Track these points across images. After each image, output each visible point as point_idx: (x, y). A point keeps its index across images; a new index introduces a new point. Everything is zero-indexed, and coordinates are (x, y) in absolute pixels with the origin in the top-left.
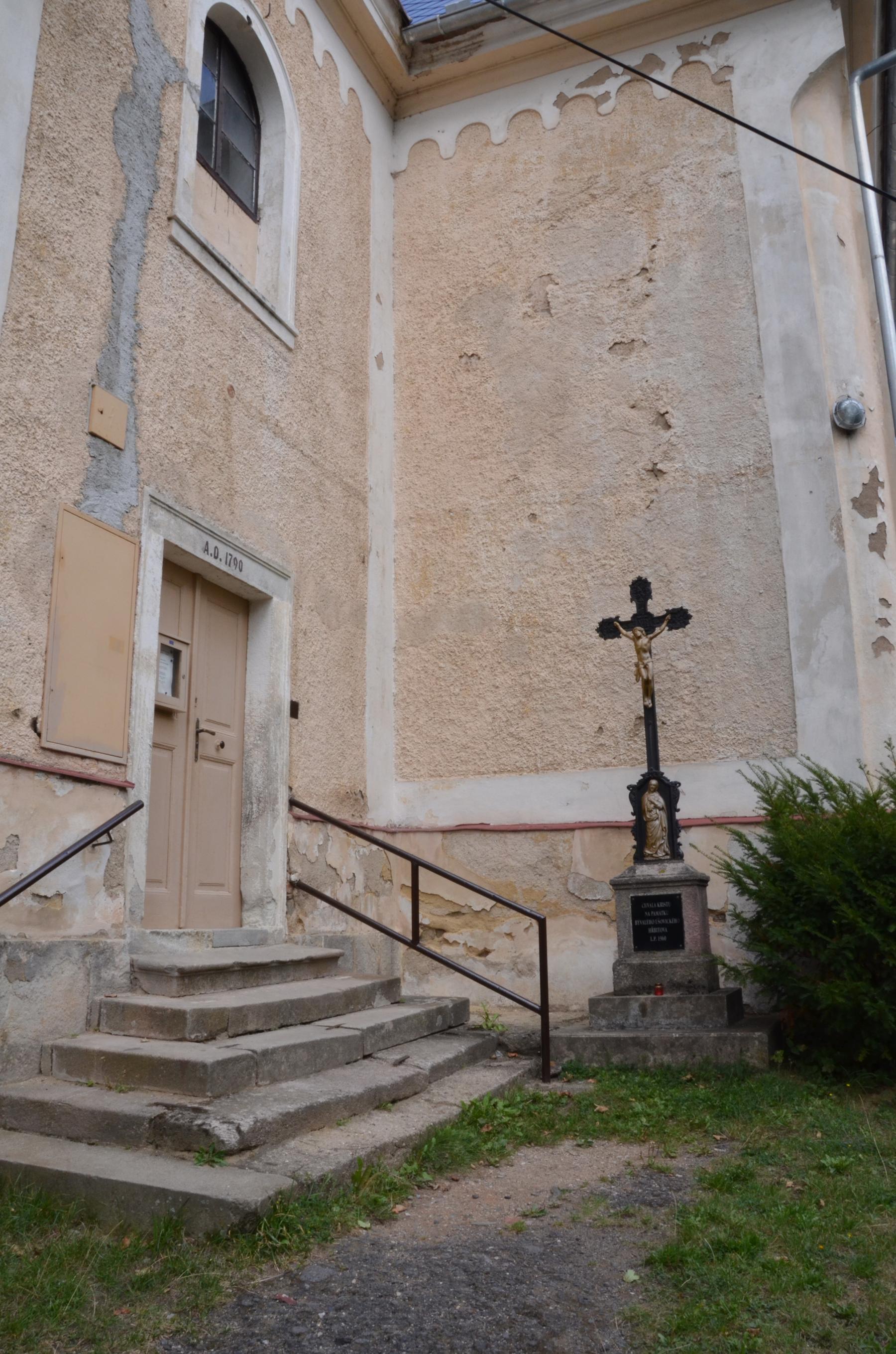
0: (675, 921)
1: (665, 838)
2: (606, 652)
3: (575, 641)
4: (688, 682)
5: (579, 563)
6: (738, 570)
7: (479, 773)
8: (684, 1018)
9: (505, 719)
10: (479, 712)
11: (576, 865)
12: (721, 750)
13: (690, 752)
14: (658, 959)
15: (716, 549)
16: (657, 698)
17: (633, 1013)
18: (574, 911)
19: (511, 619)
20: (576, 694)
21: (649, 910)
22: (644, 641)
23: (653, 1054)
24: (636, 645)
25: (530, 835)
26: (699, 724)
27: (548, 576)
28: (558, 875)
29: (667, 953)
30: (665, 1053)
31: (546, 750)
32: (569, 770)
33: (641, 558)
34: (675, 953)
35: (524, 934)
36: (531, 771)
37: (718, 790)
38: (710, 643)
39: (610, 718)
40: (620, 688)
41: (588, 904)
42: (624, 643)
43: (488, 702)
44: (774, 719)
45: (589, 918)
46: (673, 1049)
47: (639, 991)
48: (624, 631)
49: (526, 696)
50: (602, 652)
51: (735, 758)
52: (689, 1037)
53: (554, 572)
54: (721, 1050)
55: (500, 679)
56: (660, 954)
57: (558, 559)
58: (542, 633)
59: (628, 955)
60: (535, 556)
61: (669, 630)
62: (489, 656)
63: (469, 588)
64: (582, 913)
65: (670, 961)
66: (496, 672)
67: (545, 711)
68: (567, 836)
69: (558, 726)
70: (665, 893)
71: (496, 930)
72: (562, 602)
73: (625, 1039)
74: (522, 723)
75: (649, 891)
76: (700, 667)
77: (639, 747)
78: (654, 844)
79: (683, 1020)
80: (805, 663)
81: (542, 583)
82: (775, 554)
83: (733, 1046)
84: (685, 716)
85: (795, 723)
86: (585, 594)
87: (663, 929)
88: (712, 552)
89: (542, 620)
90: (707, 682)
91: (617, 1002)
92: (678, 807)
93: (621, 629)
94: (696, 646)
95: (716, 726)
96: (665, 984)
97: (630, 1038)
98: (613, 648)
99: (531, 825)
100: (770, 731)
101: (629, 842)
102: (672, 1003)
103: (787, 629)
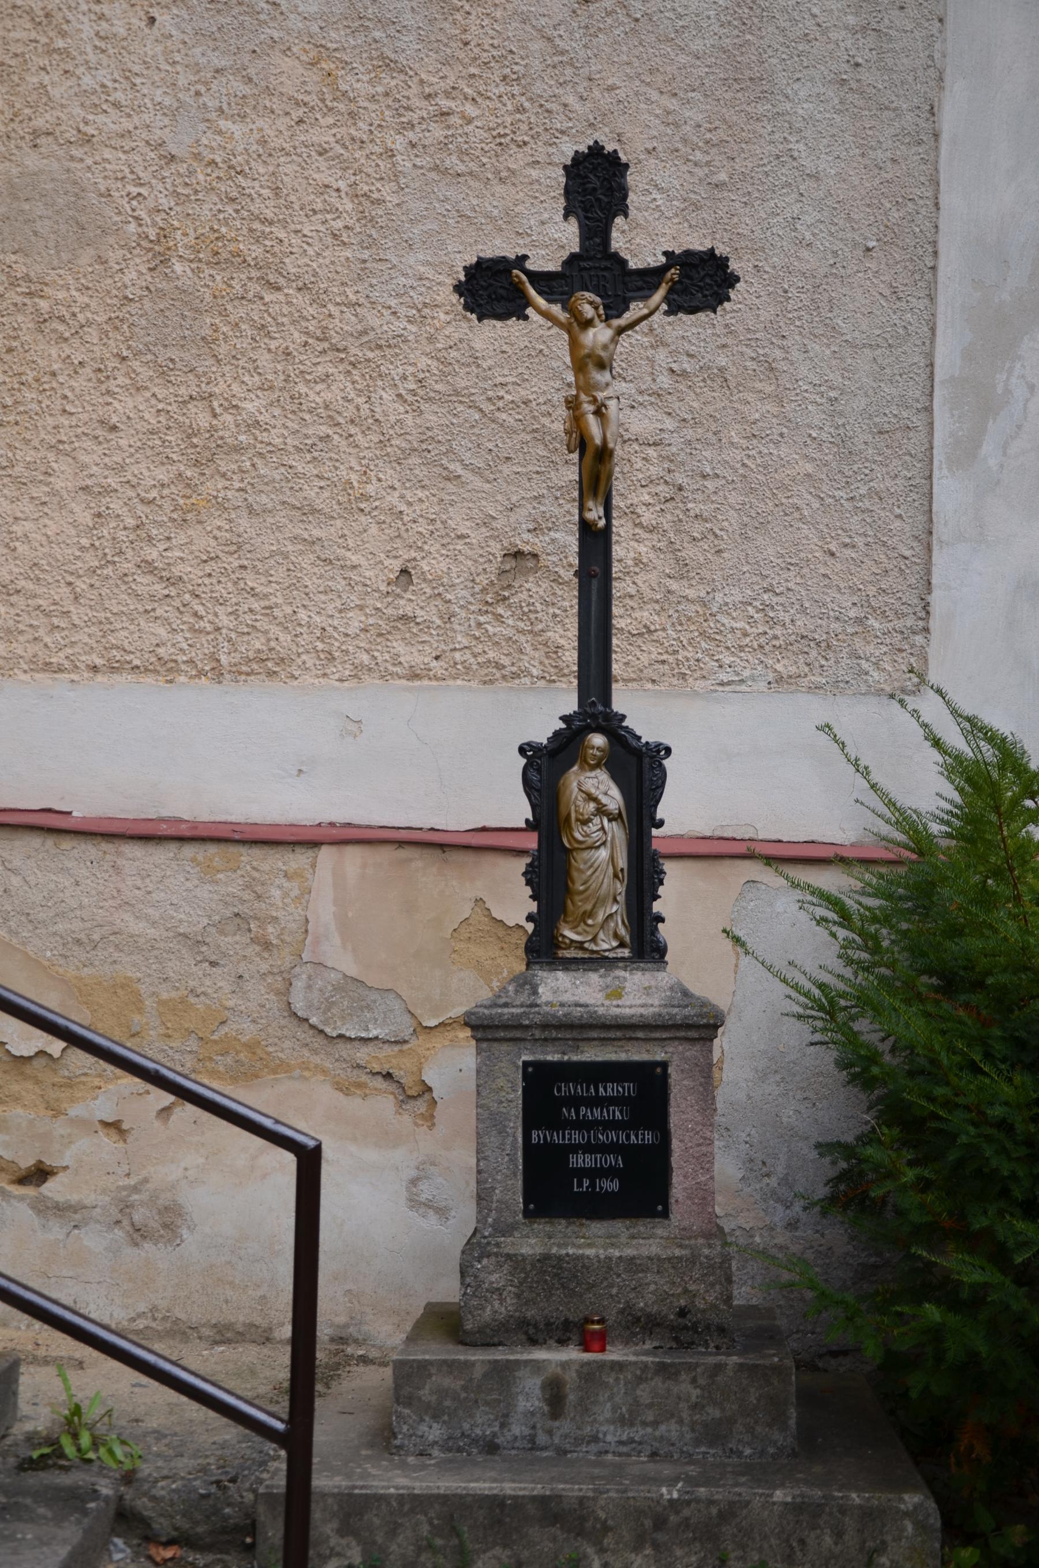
0: (649, 1137)
1: (621, 898)
2: (434, 364)
3: (348, 323)
4: (654, 471)
5: (373, 98)
6: (815, 177)
7: (48, 667)
8: (674, 1426)
9: (131, 522)
10: (54, 493)
11: (317, 942)
12: (727, 660)
13: (645, 659)
14: (595, 1242)
15: (762, 108)
17: (523, 1405)
18: (305, 1066)
19: (164, 235)
20: (343, 472)
21: (575, 1102)
22: (599, 335)
23: (602, 1551)
24: (574, 344)
25: (189, 851)
26: (674, 585)
27: (282, 123)
28: (264, 967)
29: (619, 1226)
30: (637, 1549)
31: (248, 618)
32: (308, 679)
34: (642, 1226)
35: (157, 1124)
36: (201, 673)
40: (465, 466)
41: (344, 1050)
42: (536, 336)
43: (84, 467)
44: (872, 590)
45: (343, 1088)
46: (661, 1537)
47: (535, 1334)
48: (541, 301)
49: (197, 463)
50: (423, 362)
51: (762, 685)
52: (711, 1502)
53: (300, 112)
54: (802, 1542)
55: (124, 406)
56: (597, 1228)
57: (313, 77)
58: (254, 288)
59: (505, 1230)
60: (247, 57)
61: (667, 313)
62: (92, 335)
63: (39, 123)
64: (324, 1072)
65: (629, 1252)
66: (112, 385)
68: (299, 859)
69: (286, 556)
70: (623, 1057)
71: (75, 1111)
72: (319, 206)
73: (518, 1503)
74: (182, 539)
75: (576, 1049)
76: (689, 433)
77: (508, 632)
78: (591, 914)
79: (670, 1429)
80: (967, 451)
81: (263, 142)
83: (839, 1535)
84: (638, 562)
86: (386, 191)
87: (611, 1159)
88: (749, 117)
89: (257, 251)
90: (704, 477)
91: (478, 1372)
93: (532, 292)
94: (684, 374)
95: (719, 597)
96: (612, 1317)
97: (534, 1499)
98: (454, 353)
99: (195, 824)
100: (859, 621)
101: (517, 906)
102: (640, 1380)
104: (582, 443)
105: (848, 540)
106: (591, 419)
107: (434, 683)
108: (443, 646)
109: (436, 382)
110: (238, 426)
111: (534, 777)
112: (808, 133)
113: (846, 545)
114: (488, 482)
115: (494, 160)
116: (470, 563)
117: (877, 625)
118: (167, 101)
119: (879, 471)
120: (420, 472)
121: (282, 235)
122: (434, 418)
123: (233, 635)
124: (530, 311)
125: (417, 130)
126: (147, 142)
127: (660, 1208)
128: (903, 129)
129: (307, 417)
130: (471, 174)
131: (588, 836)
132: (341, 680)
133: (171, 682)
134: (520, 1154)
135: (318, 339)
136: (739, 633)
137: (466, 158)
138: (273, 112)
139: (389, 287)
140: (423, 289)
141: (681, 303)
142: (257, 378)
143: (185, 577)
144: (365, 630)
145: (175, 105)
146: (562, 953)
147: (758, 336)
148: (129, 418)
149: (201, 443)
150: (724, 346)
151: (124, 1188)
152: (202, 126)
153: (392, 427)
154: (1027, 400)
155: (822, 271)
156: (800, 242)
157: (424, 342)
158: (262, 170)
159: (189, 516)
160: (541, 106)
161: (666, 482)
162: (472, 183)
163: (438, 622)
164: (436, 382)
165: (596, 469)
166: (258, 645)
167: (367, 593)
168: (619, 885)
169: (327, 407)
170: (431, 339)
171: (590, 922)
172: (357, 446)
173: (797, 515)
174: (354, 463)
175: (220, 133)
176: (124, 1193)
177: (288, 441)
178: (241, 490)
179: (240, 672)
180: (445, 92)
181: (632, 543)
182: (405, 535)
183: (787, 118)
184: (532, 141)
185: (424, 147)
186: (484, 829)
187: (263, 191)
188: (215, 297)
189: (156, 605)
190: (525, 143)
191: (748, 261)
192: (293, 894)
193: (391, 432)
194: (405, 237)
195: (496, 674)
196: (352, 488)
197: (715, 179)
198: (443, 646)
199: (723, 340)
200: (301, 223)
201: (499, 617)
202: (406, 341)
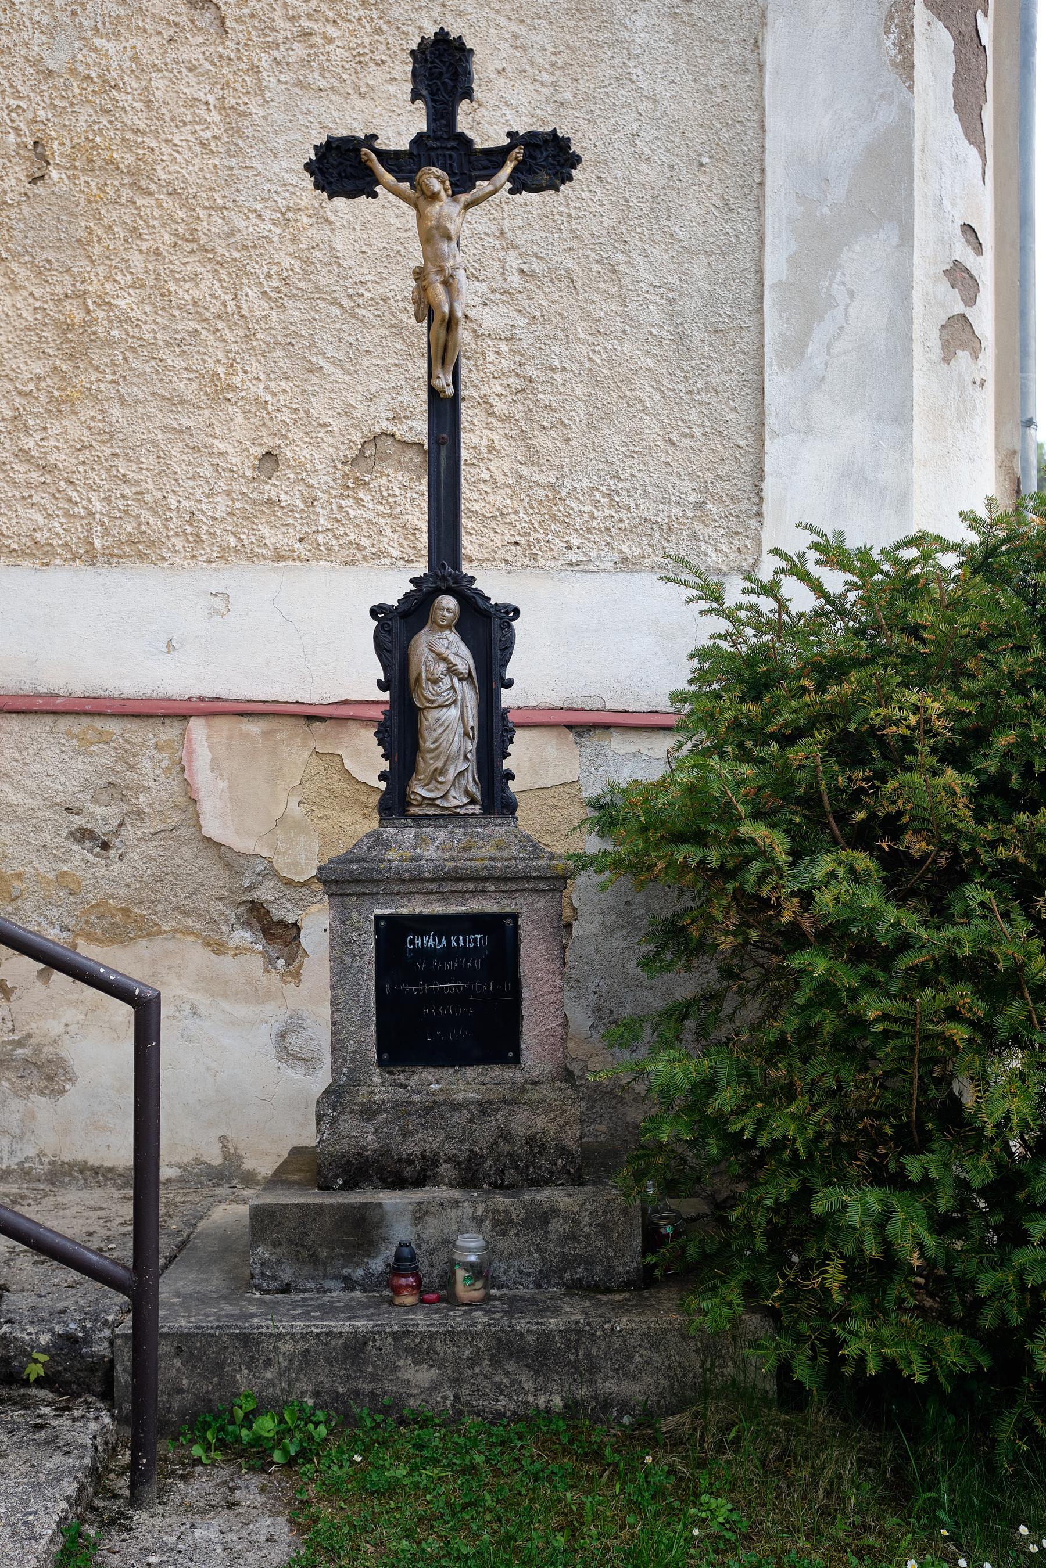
2: (297, 264)
4: (505, 364)
12: (576, 541)
15: (602, 36)
24: (421, 217)
25: (64, 723)
26: (525, 471)
31: (120, 503)
33: (410, 29)
35: (39, 984)
37: (606, 640)
39: (295, 434)
42: (384, 217)
44: (709, 477)
48: (389, 178)
50: (287, 262)
51: (609, 565)
58: (126, 193)
61: (512, 191)
68: (170, 732)
76: (539, 329)
77: (369, 515)
78: (442, 771)
80: (795, 350)
81: (135, 59)
82: (746, 71)
84: (491, 449)
85: (759, 492)
92: (510, 673)
93: (380, 169)
94: (533, 275)
101: (367, 760)
104: (426, 310)
105: (687, 431)
106: (440, 289)
107: (298, 563)
108: (306, 528)
109: (299, 280)
110: (110, 321)
111: (386, 638)
112: (644, 59)
113: (685, 435)
114: (349, 374)
115: (354, 77)
116: (332, 450)
117: (714, 509)
118: (45, 20)
119: (715, 367)
120: (285, 365)
121: (154, 144)
122: (297, 314)
123: (106, 520)
124: (378, 189)
125: (282, 48)
126: (26, 58)
127: (511, 1054)
128: (731, 59)
129: (176, 313)
130: (332, 89)
131: (438, 695)
132: (209, 562)
133: (47, 564)
134: (373, 1005)
135: (187, 240)
136: (586, 517)
137: (327, 75)
138: (145, 31)
139: (255, 192)
140: (288, 195)
142: (129, 277)
143: (60, 465)
144: (231, 514)
145: (53, 24)
146: (413, 810)
147: (602, 240)
148: (7, 315)
149: (75, 339)
150: (571, 249)
151: (10, 1043)
152: (78, 44)
153: (257, 322)
154: (847, 306)
155: (660, 184)
156: (640, 157)
157: (288, 243)
158: (135, 85)
159: (63, 407)
160: (398, 28)
161: (517, 375)
162: (333, 98)
163: (302, 506)
164: (299, 280)
165: (443, 352)
166: (129, 529)
167: (233, 479)
168: (469, 743)
169: (195, 303)
170: (294, 240)
171: (441, 779)
172: (224, 341)
173: (639, 407)
174: (221, 356)
175: (95, 50)
176: (9, 1048)
177: (159, 335)
178: (113, 382)
179: (112, 557)
180: (308, 15)
181: (486, 431)
182: (270, 424)
183: (626, 45)
184: (389, 60)
185: (288, 64)
186: (347, 702)
187: (135, 104)
188: (89, 202)
189: (33, 492)
190: (383, 62)
191: (592, 172)
192: (163, 765)
193: (257, 326)
194: (270, 146)
195: (355, 557)
196: (219, 379)
197: (558, 97)
198: (306, 528)
199: (570, 244)
200: (171, 133)
201: (359, 501)
202: (270, 242)
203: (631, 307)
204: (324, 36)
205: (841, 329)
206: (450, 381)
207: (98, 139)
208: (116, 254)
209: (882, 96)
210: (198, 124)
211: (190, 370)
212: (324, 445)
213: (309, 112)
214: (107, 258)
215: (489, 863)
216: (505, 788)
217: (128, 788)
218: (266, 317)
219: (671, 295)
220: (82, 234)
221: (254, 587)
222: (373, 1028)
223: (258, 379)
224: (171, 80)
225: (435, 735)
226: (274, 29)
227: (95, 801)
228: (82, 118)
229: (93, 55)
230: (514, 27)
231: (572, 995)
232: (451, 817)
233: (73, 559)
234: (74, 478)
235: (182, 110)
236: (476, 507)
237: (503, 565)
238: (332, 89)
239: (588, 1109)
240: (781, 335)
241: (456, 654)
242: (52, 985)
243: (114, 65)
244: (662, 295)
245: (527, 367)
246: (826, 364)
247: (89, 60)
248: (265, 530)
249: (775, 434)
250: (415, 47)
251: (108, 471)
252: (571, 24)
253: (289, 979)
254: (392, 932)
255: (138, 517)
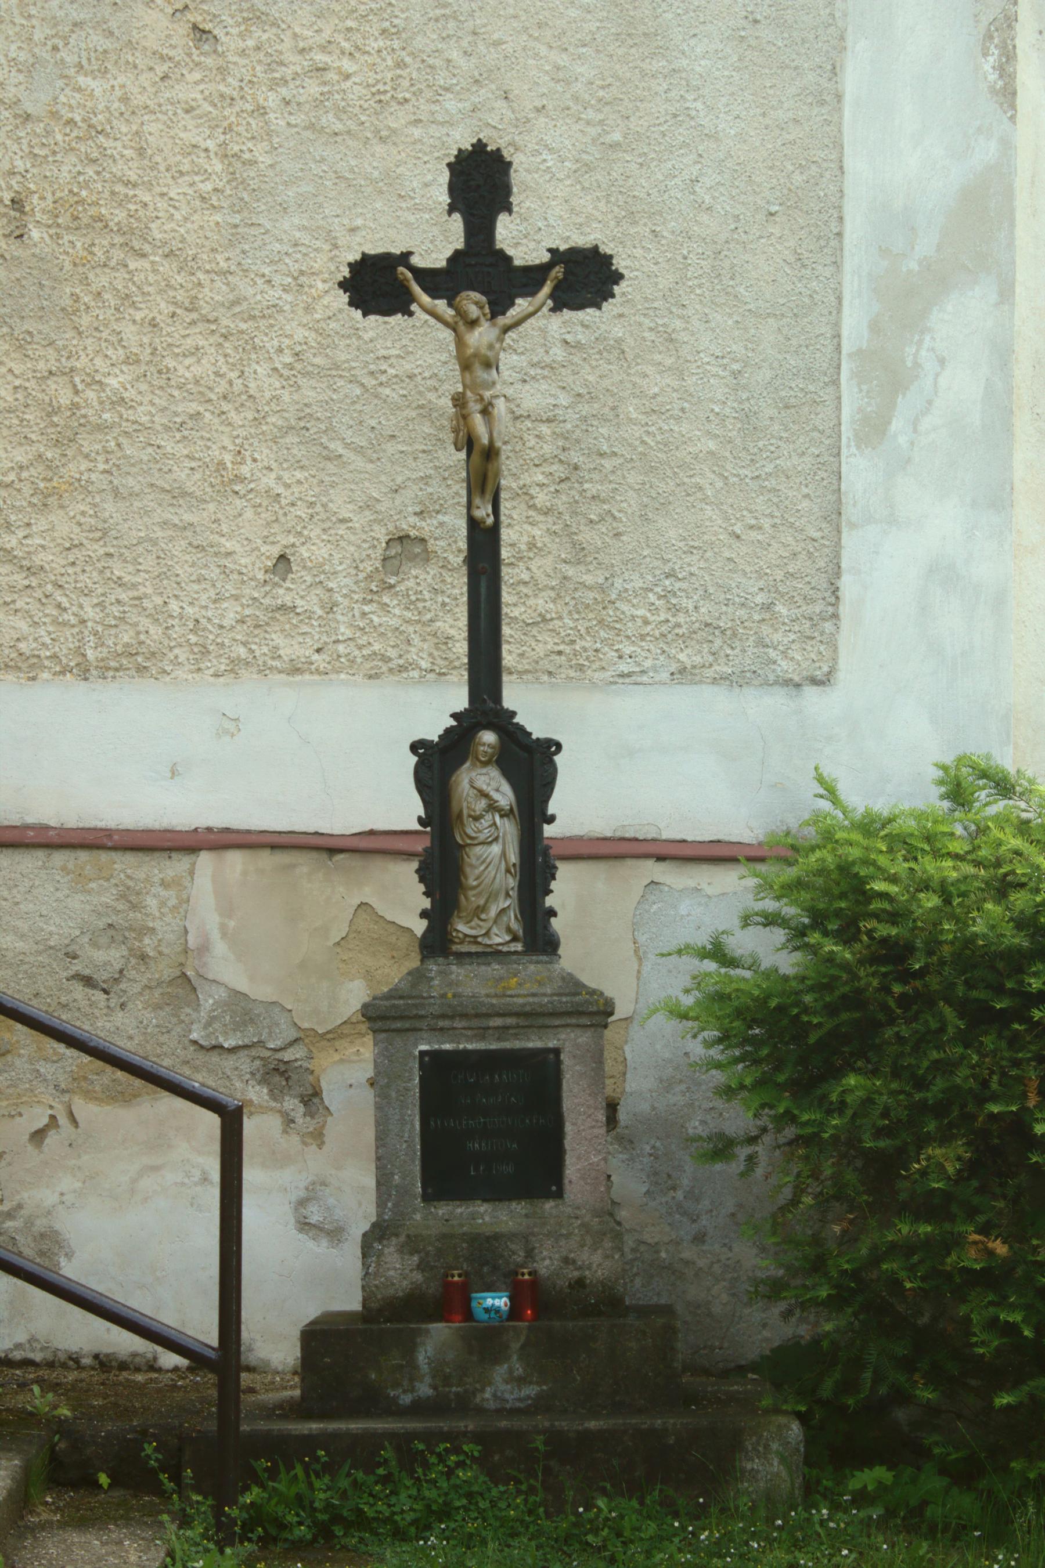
4: (548, 449)
5: (243, 53)
12: (628, 650)
13: (541, 650)
15: (658, 64)
16: (505, 506)
24: (460, 342)
25: (59, 858)
26: (570, 571)
27: (145, 79)
31: (116, 610)
35: (30, 1148)
38: (619, 341)
39: (314, 532)
40: (347, 445)
42: (418, 344)
44: (779, 575)
48: (425, 299)
50: (300, 334)
51: (665, 676)
58: (117, 254)
61: (553, 310)
67: (116, 493)
68: (177, 866)
69: (155, 542)
76: (585, 409)
77: (394, 622)
80: (874, 429)
81: (125, 99)
82: (822, 103)
84: (532, 545)
90: (602, 455)
92: (552, 808)
93: (416, 289)
94: (578, 346)
98: (333, 325)
99: (62, 830)
100: (768, 607)
101: (402, 898)
103: (837, 325)
105: (753, 522)
107: (316, 677)
108: (324, 638)
110: (101, 403)
113: (752, 527)
114: (371, 461)
116: (352, 549)
117: (784, 611)
118: (23, 56)
121: (147, 198)
124: (414, 307)
129: (176, 393)
133: (34, 679)
134: (418, 1140)
138: (135, 67)
139: (263, 253)
141: (561, 301)
142: (121, 351)
143: (47, 567)
145: (31, 60)
150: (621, 316)
153: (268, 403)
154: (937, 375)
155: (723, 237)
156: (700, 206)
160: (423, 61)
162: (350, 143)
163: (320, 612)
166: (126, 639)
167: (243, 582)
169: (197, 382)
170: (308, 309)
171: (483, 916)
172: (230, 424)
174: (227, 442)
175: (79, 90)
177: (156, 419)
179: (106, 670)
181: (526, 526)
184: (414, 99)
185: (299, 104)
186: (372, 833)
189: (16, 596)
190: (406, 100)
191: (645, 225)
192: (170, 904)
194: (279, 200)
195: (381, 669)
197: (608, 139)
198: (324, 638)
202: (281, 311)
203: (690, 381)
204: (339, 71)
205: (930, 402)
206: (490, 510)
207: (84, 193)
208: (106, 326)
209: (979, 129)
210: (197, 174)
211: (193, 459)
212: (342, 543)
213: (323, 160)
214: (96, 329)
215: (531, 1000)
216: (547, 925)
217: (131, 929)
218: (277, 398)
219: (736, 367)
220: (67, 302)
221: (271, 709)
222: (418, 1162)
223: (270, 469)
224: (165, 123)
225: (477, 872)
226: (281, 63)
227: (94, 944)
228: (65, 168)
229: (77, 95)
230: (554, 56)
231: (625, 1156)
232: (495, 954)
233: (62, 673)
234: (62, 581)
235: (179, 157)
236: (515, 612)
237: (545, 678)
238: (349, 132)
239: (643, 1286)
240: (860, 410)
241: (497, 790)
242: (45, 1148)
243: (101, 107)
244: (725, 367)
245: (572, 453)
246: (912, 443)
247: (73, 102)
248: (278, 639)
249: (853, 526)
250: (452, 159)
251: (101, 572)
252: (621, 52)
253: (309, 1140)
254: (438, 1069)
255: (136, 624)
